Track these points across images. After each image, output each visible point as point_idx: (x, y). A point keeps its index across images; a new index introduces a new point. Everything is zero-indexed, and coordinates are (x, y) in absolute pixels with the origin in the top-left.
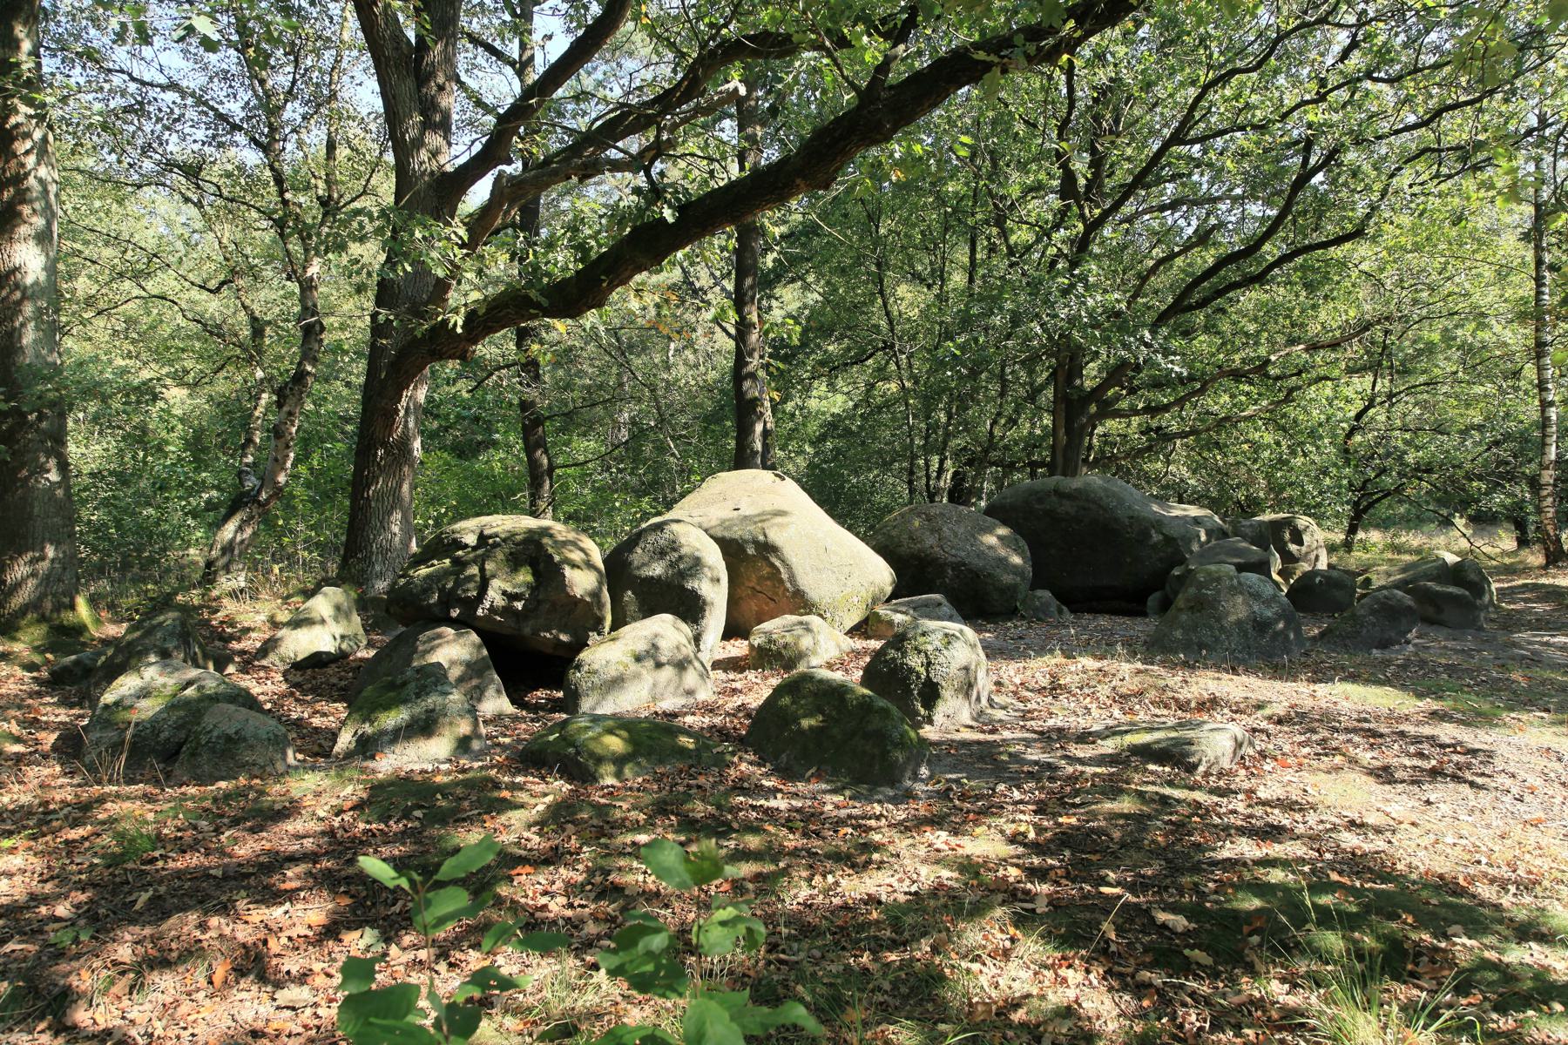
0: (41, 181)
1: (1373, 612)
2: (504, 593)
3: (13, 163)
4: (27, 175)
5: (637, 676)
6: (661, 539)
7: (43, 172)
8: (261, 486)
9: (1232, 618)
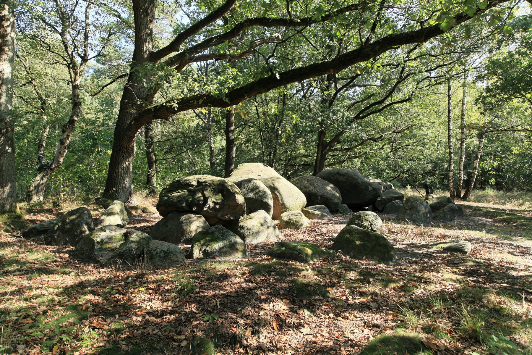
0: (12, 38)
1: (449, 211)
2: (213, 202)
3: (2, 30)
4: (7, 35)
5: (263, 231)
6: (251, 185)
7: (13, 35)
8: (53, 163)
9: (421, 212)
